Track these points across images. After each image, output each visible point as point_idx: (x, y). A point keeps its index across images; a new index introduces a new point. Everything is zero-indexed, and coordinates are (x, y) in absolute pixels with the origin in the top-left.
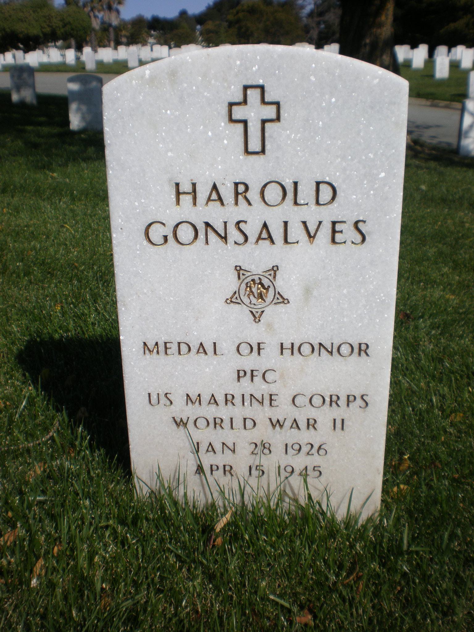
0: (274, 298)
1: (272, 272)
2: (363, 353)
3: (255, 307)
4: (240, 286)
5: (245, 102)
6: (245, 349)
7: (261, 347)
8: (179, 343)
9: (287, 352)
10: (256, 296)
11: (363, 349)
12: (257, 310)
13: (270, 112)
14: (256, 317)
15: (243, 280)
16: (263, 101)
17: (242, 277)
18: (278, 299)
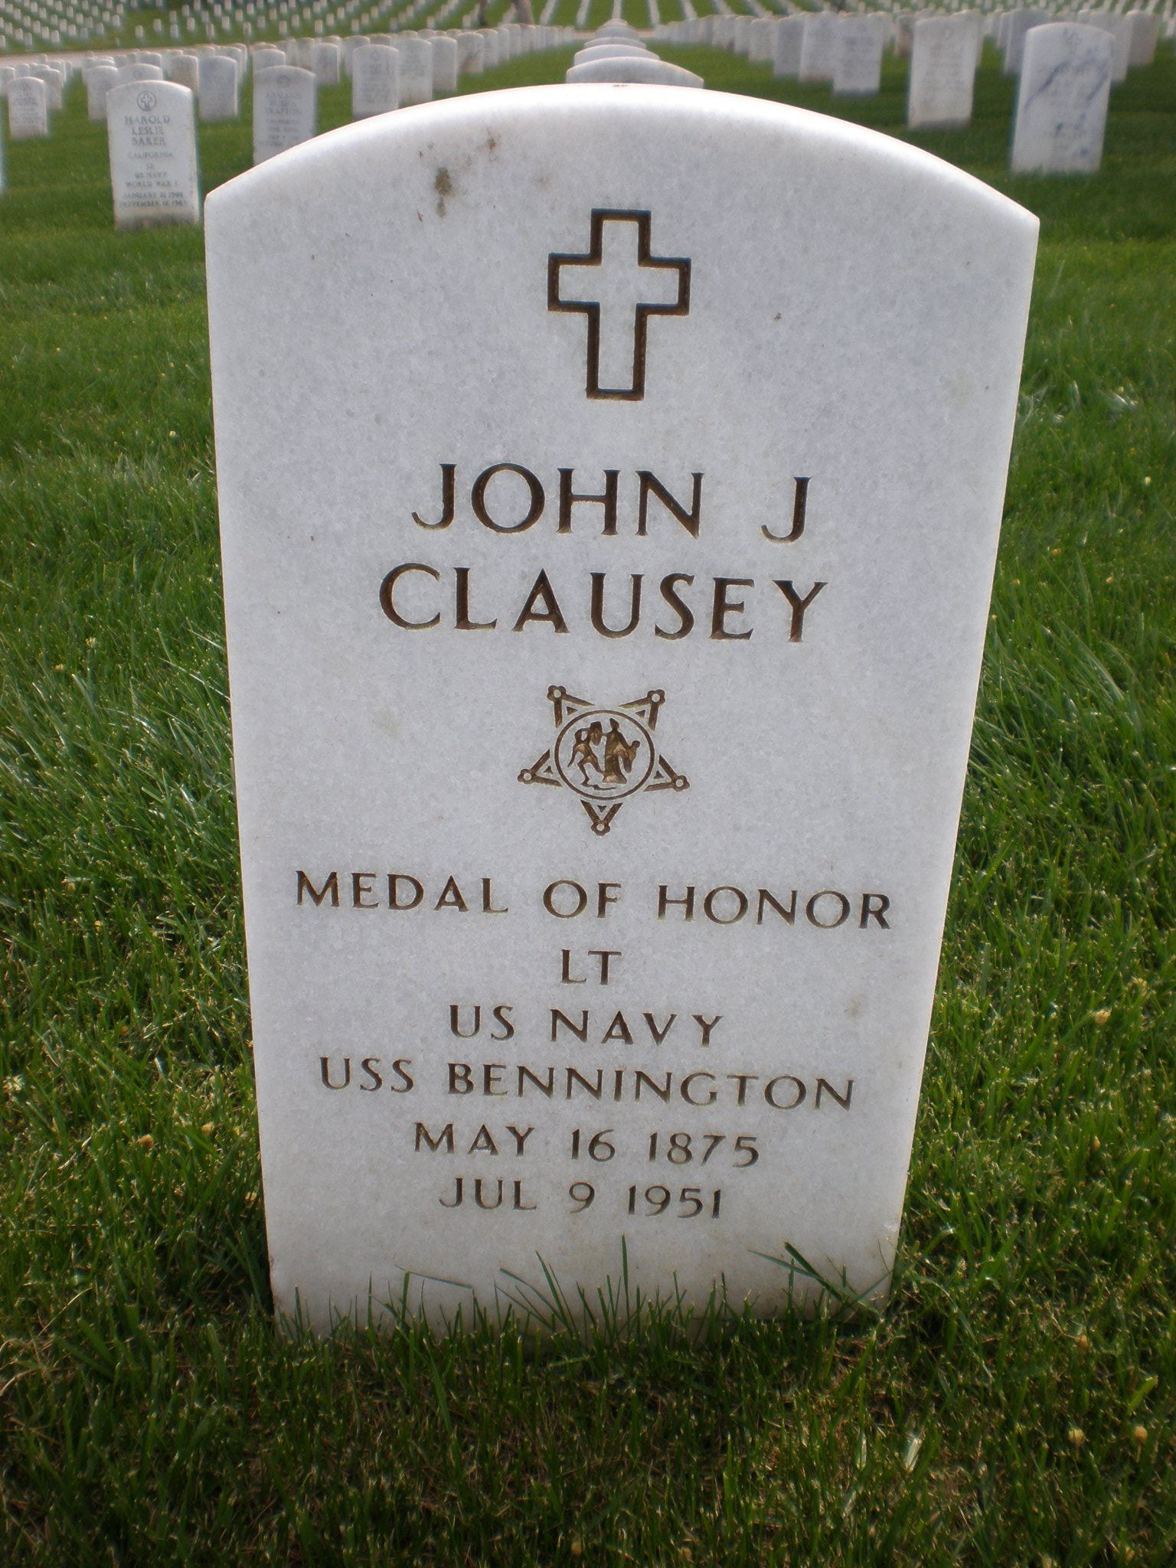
0: (648, 774)
1: (647, 707)
2: (872, 919)
3: (601, 793)
4: (559, 740)
5: (595, 256)
6: (565, 899)
7: (608, 895)
8: (393, 879)
9: (675, 911)
10: (602, 766)
11: (875, 910)
12: (603, 803)
13: (662, 286)
14: (601, 820)
15: (570, 725)
16: (645, 257)
17: (567, 718)
18: (658, 775)
